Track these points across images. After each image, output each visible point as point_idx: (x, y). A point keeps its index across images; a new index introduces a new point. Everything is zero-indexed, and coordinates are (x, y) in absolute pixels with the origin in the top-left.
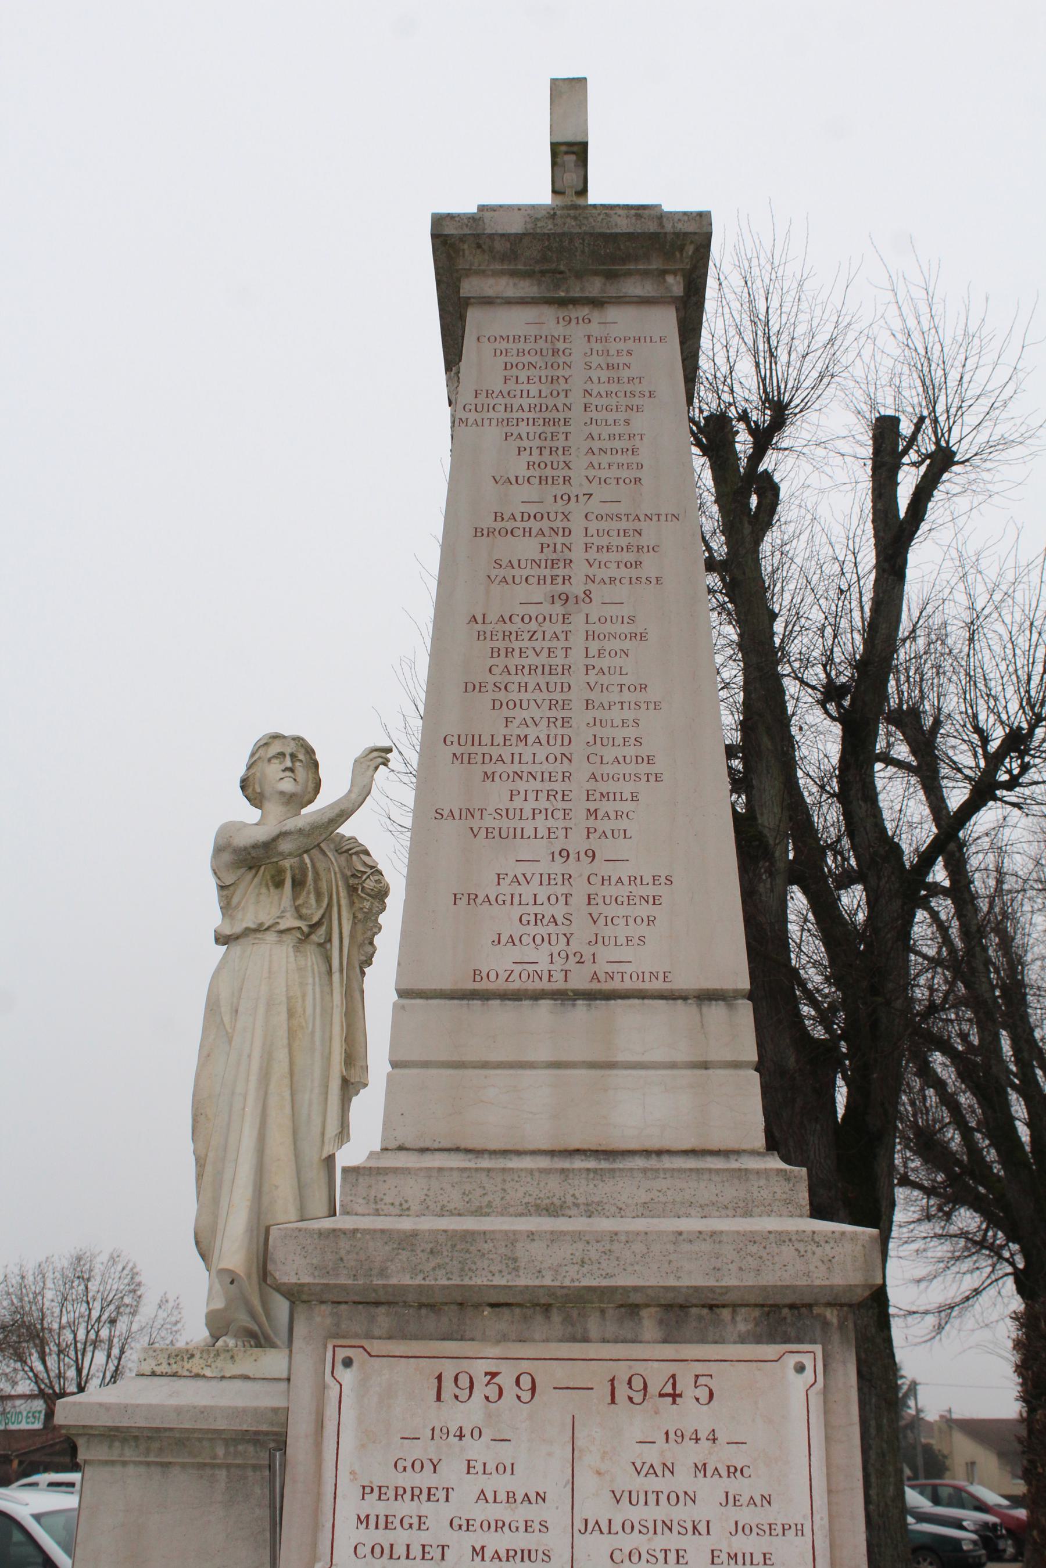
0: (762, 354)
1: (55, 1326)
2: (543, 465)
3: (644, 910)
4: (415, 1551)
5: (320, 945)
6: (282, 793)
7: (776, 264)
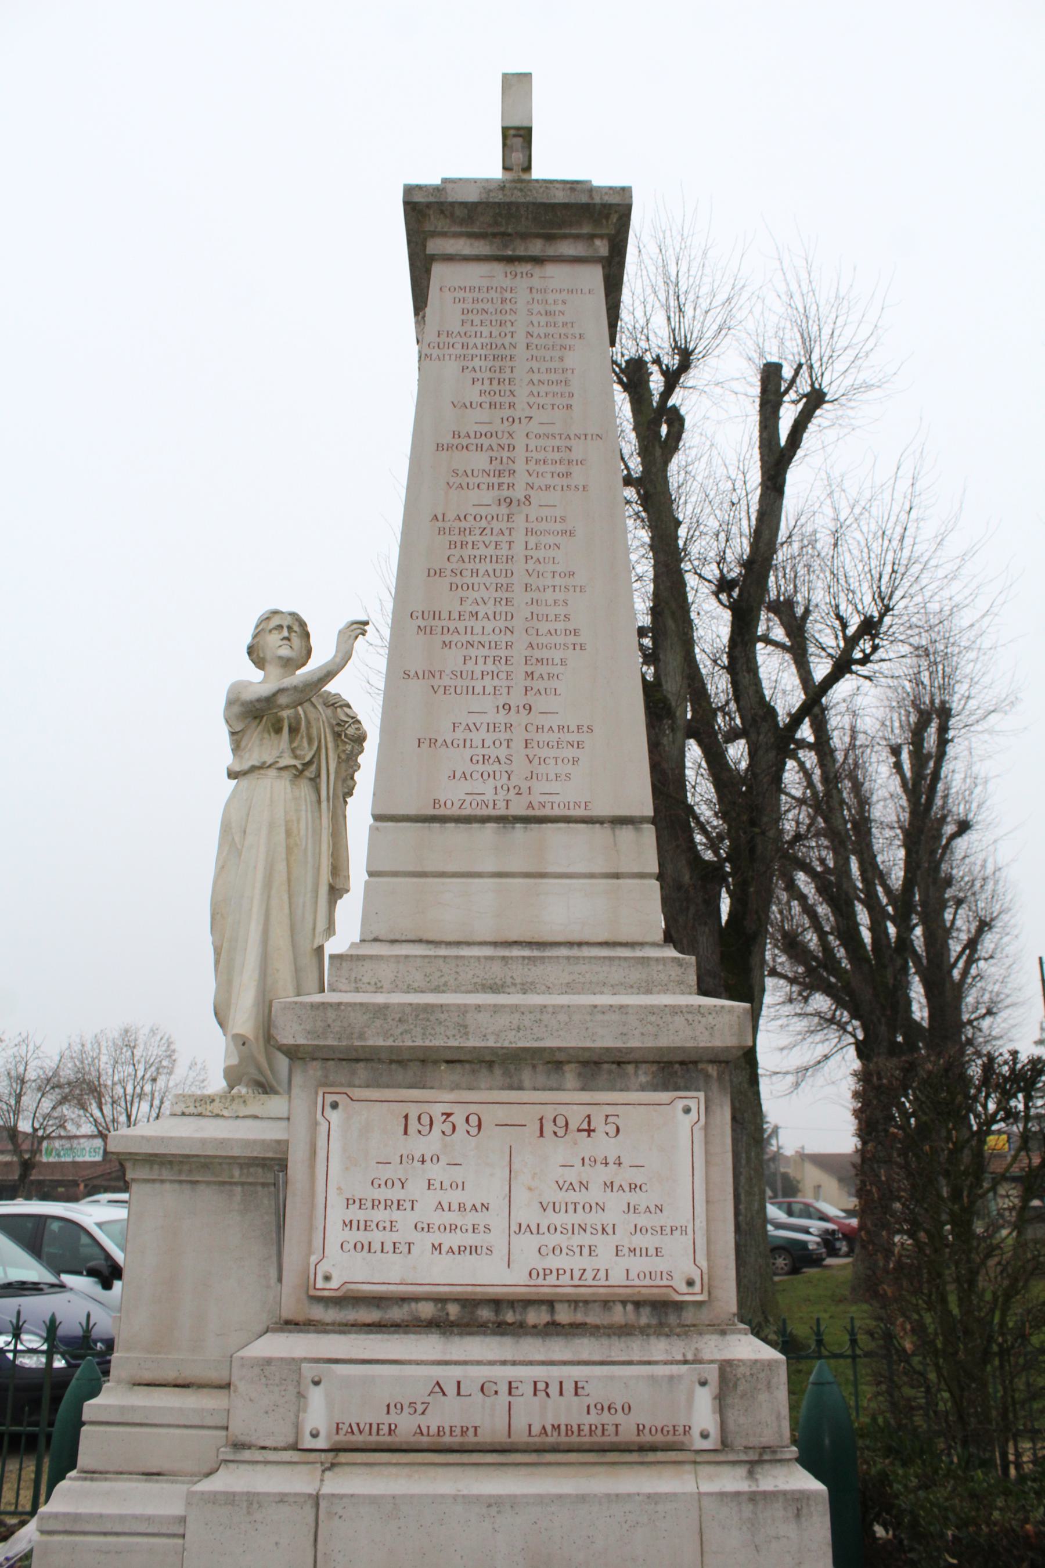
0: (672, 309)
1: (109, 1083)
2: (492, 393)
3: (570, 753)
4: (389, 1247)
5: (311, 779)
6: (280, 658)
7: (685, 236)
